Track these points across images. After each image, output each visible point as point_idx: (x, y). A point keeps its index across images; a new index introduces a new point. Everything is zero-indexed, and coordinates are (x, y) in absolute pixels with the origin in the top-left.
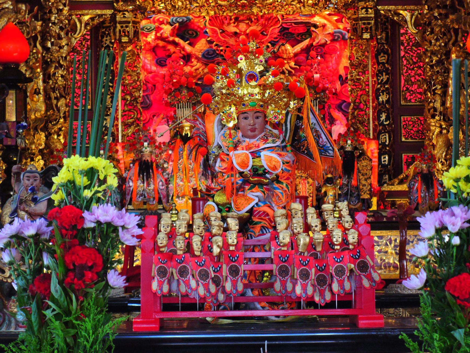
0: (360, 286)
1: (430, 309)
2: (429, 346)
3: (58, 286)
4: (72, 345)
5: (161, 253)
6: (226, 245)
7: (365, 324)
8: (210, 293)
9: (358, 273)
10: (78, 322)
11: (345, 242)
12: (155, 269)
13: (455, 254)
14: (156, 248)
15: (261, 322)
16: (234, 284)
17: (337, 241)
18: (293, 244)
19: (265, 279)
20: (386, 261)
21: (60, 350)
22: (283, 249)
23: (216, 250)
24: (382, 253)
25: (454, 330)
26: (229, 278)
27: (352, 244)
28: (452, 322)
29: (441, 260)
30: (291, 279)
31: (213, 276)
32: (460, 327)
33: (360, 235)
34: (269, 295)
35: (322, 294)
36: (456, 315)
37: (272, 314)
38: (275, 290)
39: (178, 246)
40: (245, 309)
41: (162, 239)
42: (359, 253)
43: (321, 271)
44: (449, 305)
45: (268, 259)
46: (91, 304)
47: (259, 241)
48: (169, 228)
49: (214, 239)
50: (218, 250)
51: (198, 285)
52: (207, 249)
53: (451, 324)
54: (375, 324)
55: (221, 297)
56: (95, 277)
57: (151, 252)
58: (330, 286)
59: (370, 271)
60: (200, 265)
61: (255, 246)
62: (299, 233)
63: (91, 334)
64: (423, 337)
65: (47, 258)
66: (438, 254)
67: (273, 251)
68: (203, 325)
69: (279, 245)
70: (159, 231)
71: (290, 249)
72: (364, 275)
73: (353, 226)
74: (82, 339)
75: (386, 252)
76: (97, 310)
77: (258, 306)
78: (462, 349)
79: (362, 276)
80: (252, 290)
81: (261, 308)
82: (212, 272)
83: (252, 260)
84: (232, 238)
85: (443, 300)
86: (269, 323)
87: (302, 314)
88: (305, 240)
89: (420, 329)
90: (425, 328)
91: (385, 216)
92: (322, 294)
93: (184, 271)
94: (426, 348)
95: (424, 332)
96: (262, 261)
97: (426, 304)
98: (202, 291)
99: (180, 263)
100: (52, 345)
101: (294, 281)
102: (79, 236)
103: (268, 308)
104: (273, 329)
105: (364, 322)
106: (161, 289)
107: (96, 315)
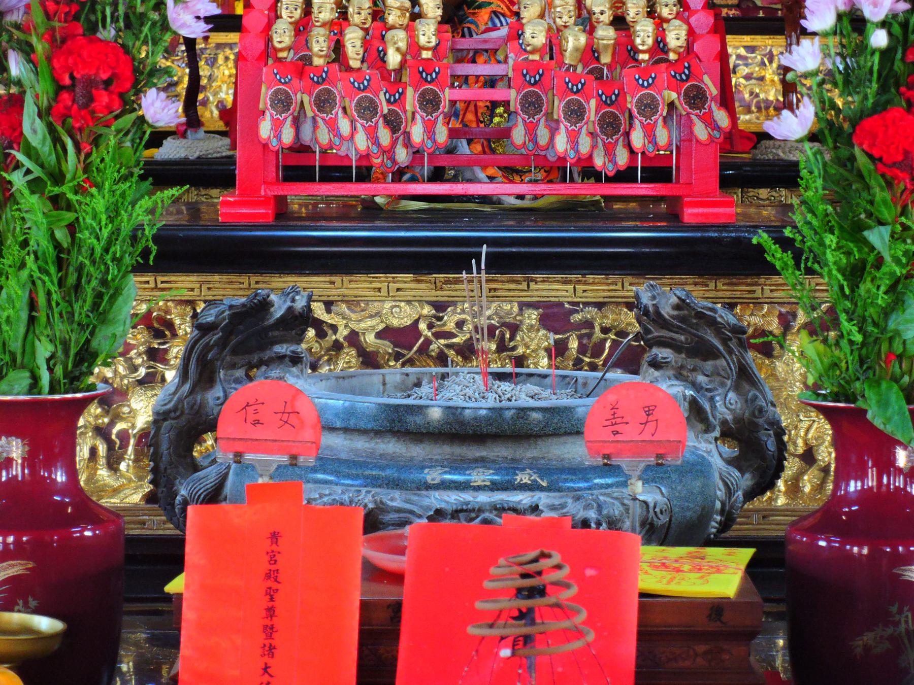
0: (689, 137)
1: (820, 182)
2: (816, 260)
3: (38, 120)
4: (65, 245)
5: (279, 60)
6: (414, 47)
7: (697, 215)
8: (379, 146)
9: (685, 110)
10: (78, 197)
11: (660, 46)
12: (266, 94)
13: (876, 68)
14: (268, 51)
15: (487, 209)
16: (430, 129)
17: (643, 44)
18: (553, 46)
19: (496, 120)
20: (762, 96)
21: (39, 254)
22: (531, 57)
23: (393, 59)
24: (753, 81)
25: (869, 228)
26: (418, 117)
27: (675, 51)
28: (865, 211)
29: (849, 81)
30: (546, 120)
31: (386, 111)
32: (881, 223)
33: (691, 33)
34: (504, 154)
35: (610, 151)
36: (874, 196)
37: (508, 192)
38: (513, 143)
39: (316, 48)
40: (454, 180)
41: (282, 35)
42: (688, 68)
43: (609, 106)
44: (860, 176)
45: (502, 77)
46: (107, 159)
47: (485, 41)
48: (299, 11)
49: (389, 35)
50: (398, 58)
51: (354, 130)
52: (374, 53)
53: (863, 216)
54: (716, 215)
55: (402, 156)
56: (117, 103)
57: (259, 59)
58: (627, 135)
59: (710, 107)
60: (359, 88)
61: (477, 52)
62: (565, 27)
63: (103, 223)
64: (803, 241)
65: (17, 63)
66: (841, 67)
67: (511, 62)
68: (370, 211)
69: (525, 50)
70: (278, 17)
71: (547, 57)
72: (697, 115)
73: (678, 13)
74: (87, 233)
75: (762, 79)
76: (118, 172)
77: (482, 175)
78: (884, 269)
79: (693, 117)
80: (470, 142)
81: (487, 180)
82: (384, 103)
83: (471, 80)
84: (427, 33)
85: (849, 164)
86: (501, 209)
87: (568, 192)
88: (577, 40)
89: (799, 225)
90: (809, 223)
91: (761, 8)
92: (610, 151)
93: (326, 101)
94: (809, 264)
95: (806, 231)
96: (491, 82)
97: (811, 173)
98: (362, 141)
99: (318, 83)
100: (25, 244)
101: (553, 125)
102: (83, 17)
103: (500, 179)
104: (511, 223)
105: (696, 210)
106: (278, 136)
107: (116, 182)
